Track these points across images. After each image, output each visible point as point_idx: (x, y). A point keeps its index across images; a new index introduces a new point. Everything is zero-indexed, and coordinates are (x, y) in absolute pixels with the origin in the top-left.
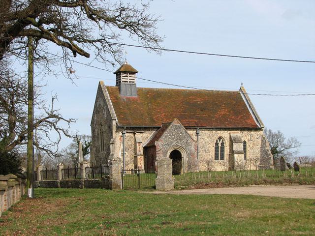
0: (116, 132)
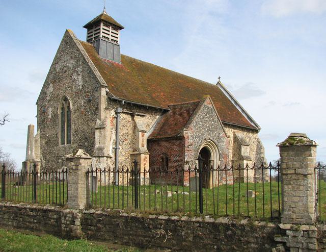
0: (107, 109)
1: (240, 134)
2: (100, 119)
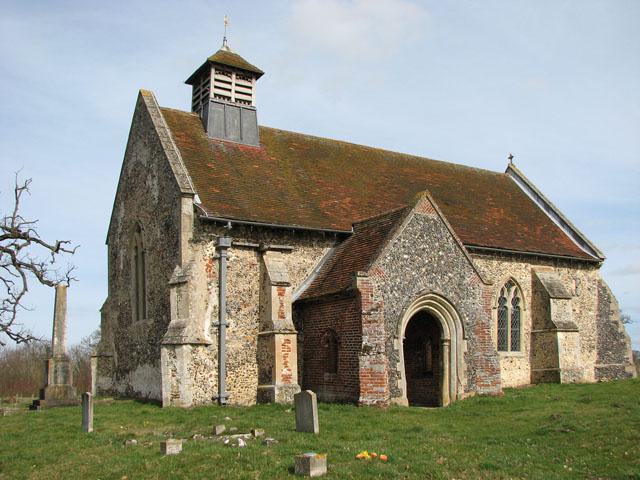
0: (195, 241)
1: (548, 274)
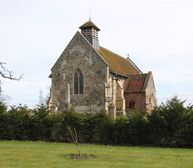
2: (107, 83)
